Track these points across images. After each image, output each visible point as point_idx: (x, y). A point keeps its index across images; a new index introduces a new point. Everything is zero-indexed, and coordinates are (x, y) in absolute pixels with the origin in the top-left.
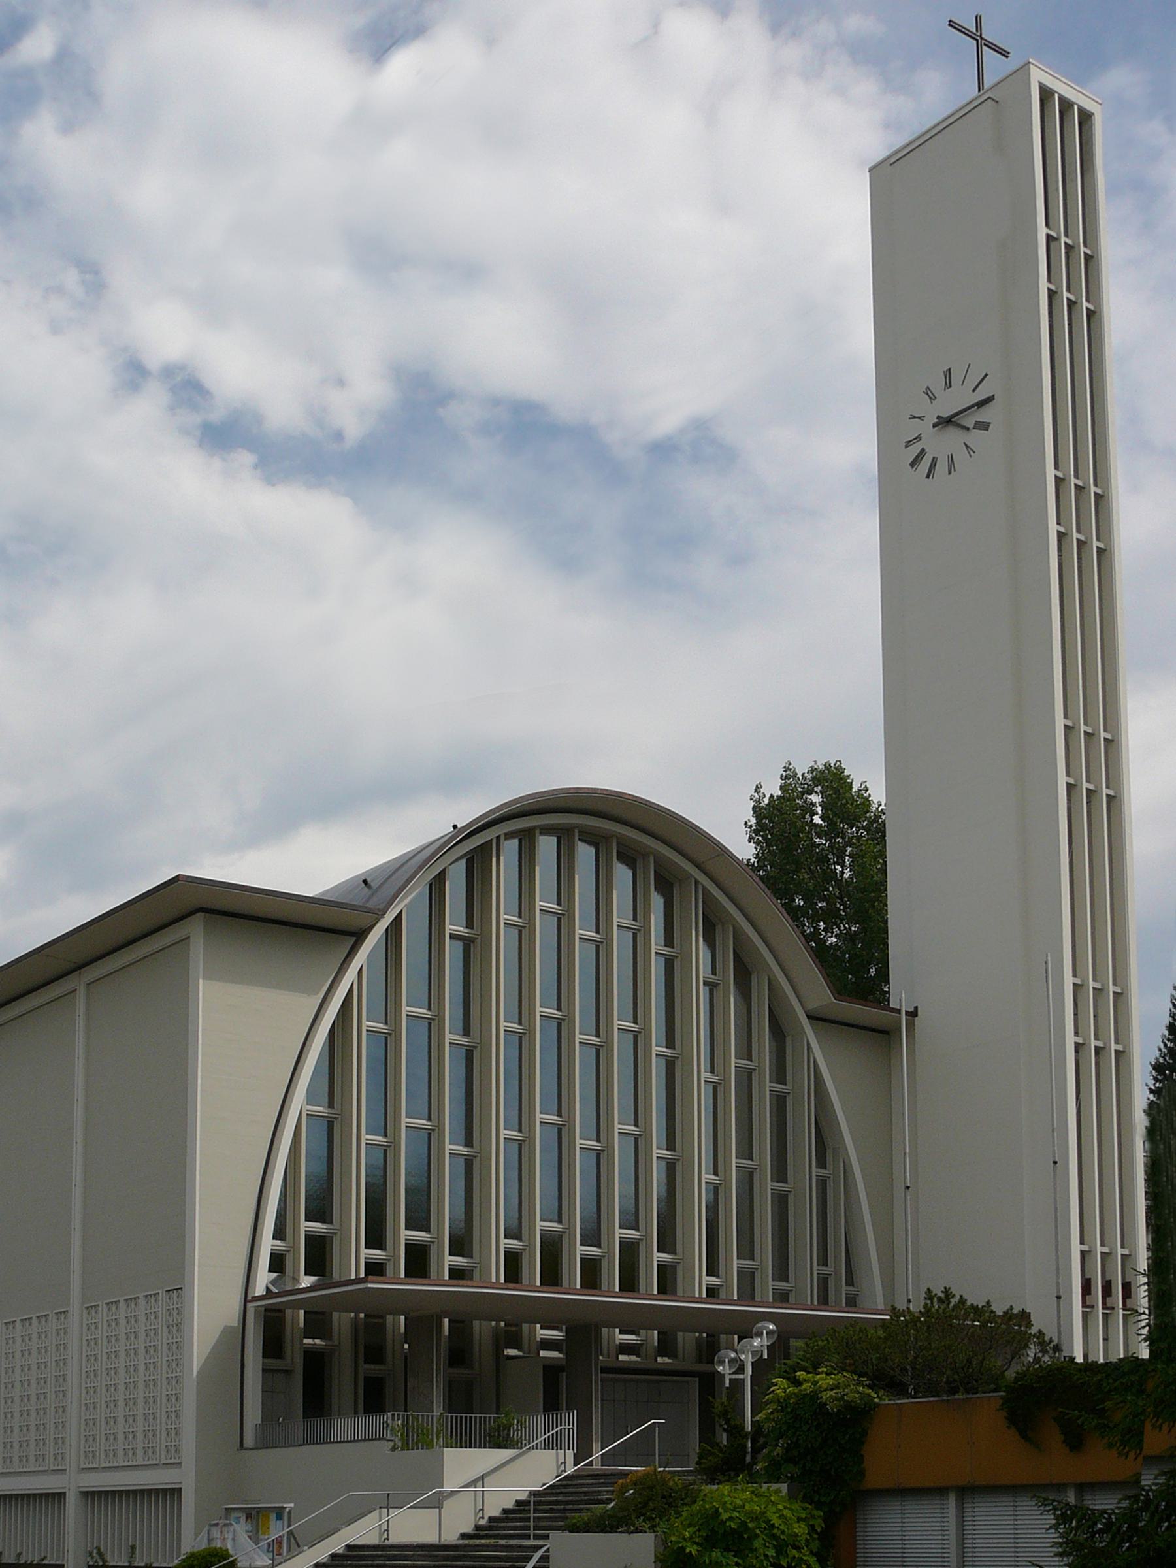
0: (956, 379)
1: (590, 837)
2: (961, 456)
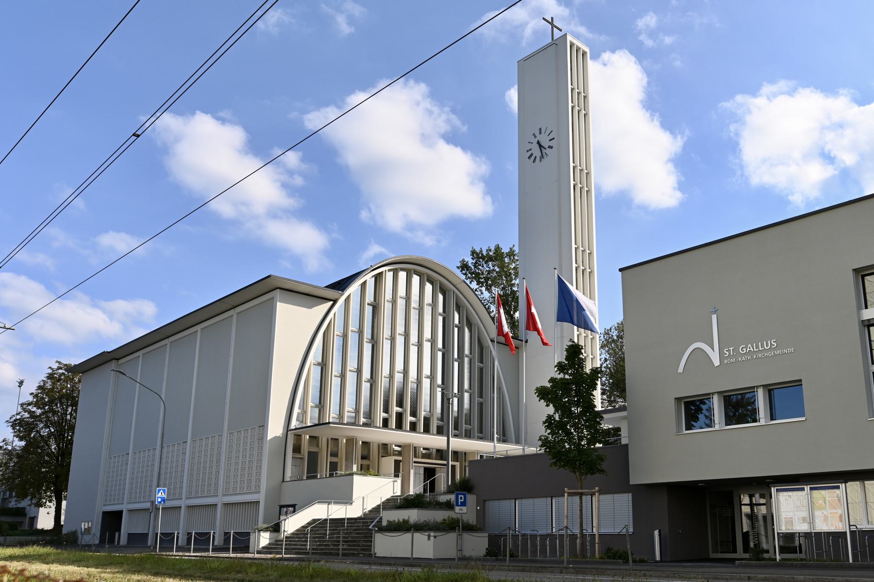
0: (543, 132)
1: (417, 273)
2: (537, 133)
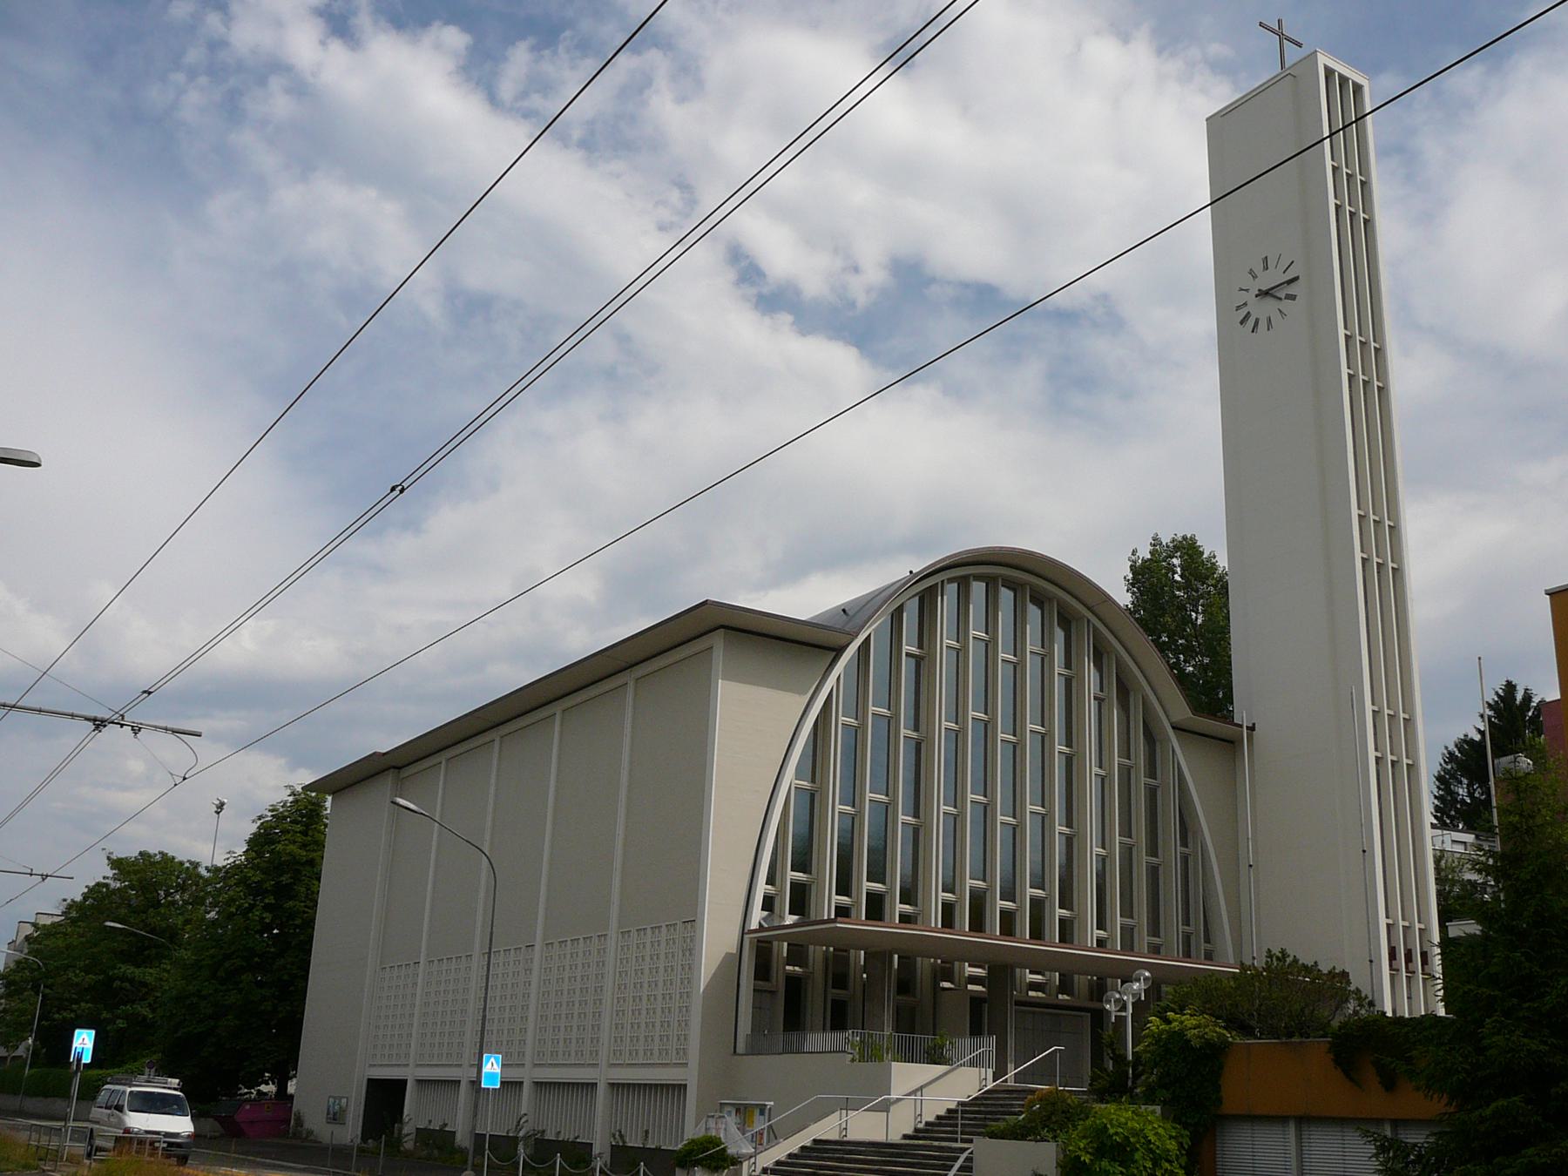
2: (1258, 268)
